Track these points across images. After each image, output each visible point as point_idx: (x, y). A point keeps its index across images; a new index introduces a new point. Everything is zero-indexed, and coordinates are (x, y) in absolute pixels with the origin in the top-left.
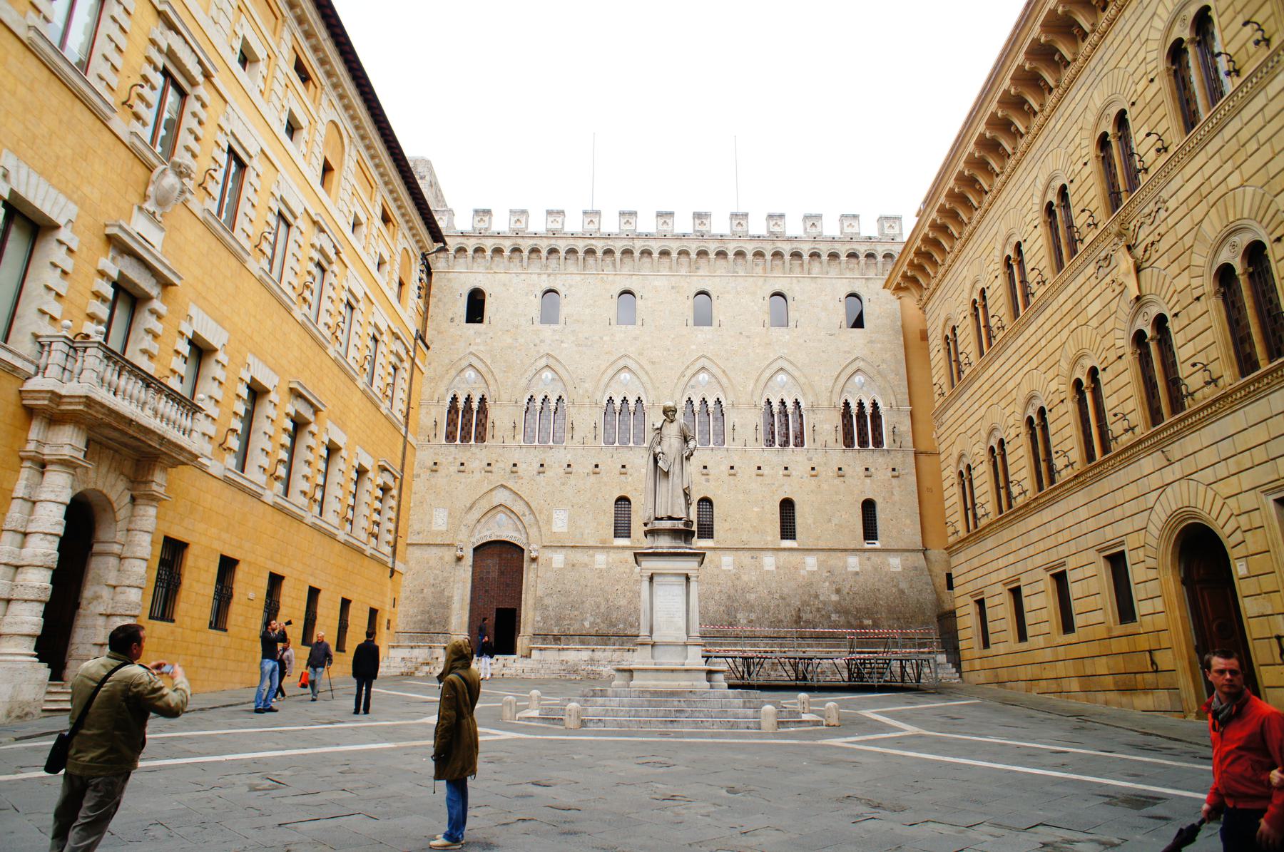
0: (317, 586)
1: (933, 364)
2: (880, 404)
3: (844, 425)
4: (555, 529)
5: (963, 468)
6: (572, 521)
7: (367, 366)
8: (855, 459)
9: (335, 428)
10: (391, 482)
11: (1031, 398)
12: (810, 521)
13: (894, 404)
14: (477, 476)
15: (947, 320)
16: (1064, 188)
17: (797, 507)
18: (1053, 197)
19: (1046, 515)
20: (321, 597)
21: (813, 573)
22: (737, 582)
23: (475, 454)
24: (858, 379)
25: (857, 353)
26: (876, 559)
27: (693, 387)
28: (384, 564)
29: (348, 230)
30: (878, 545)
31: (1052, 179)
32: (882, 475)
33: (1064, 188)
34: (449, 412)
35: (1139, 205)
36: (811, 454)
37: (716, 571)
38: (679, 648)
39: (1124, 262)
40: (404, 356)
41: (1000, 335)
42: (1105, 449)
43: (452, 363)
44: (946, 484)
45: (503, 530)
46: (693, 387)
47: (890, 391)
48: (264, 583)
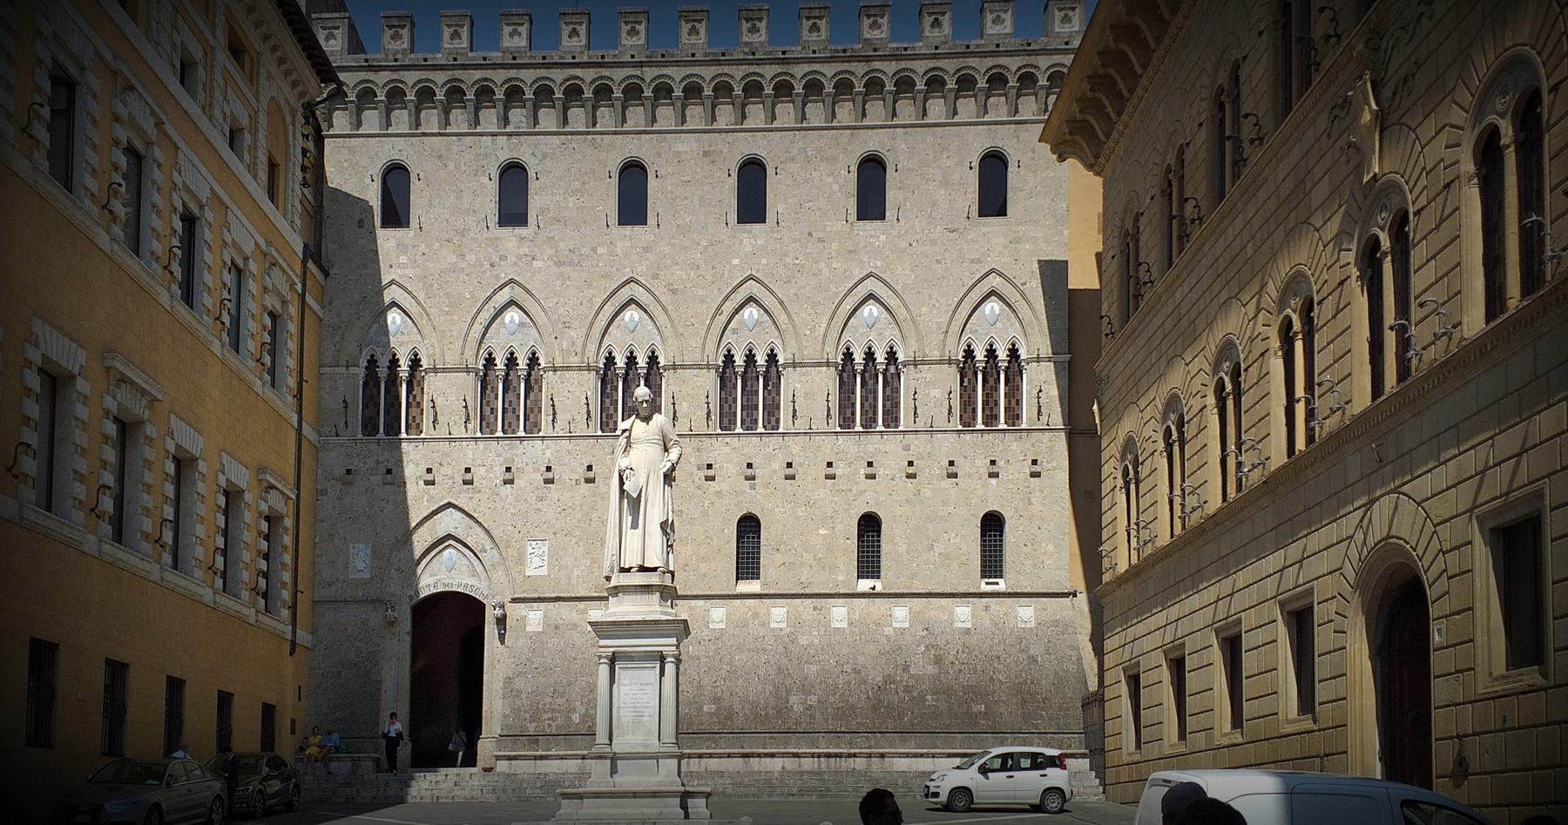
6: (554, 558)
12: (902, 549)
17: (885, 528)
27: (735, 331)
34: (365, 384)
46: (735, 331)
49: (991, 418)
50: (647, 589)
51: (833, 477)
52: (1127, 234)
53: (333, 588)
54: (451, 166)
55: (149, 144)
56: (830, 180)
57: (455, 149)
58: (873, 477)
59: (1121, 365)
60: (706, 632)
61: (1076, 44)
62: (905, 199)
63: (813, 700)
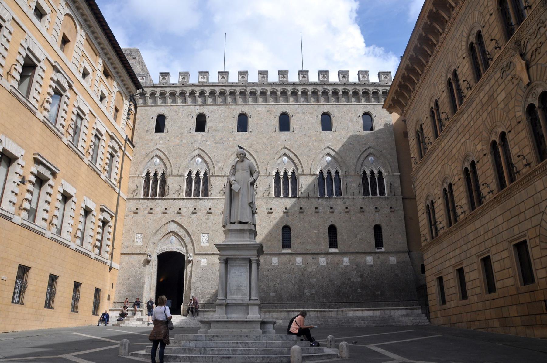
0: (55, 273)
1: (411, 147)
2: (383, 172)
3: (363, 184)
4: (202, 244)
5: (429, 203)
7: (91, 151)
8: (369, 204)
9: (68, 184)
10: (108, 218)
11: (465, 158)
12: (345, 237)
13: (390, 171)
14: (160, 215)
15: (417, 121)
16: (479, 33)
17: (338, 230)
18: (473, 39)
19: (478, 224)
20: (59, 281)
21: (347, 266)
22: (305, 272)
23: (159, 205)
24: (370, 158)
25: (370, 144)
26: (382, 257)
28: (106, 263)
29: (79, 76)
30: (383, 250)
31: (472, 29)
32: (385, 211)
33: (479, 33)
35: (526, 32)
36: (346, 200)
37: (293, 267)
38: (244, 307)
39: (519, 64)
40: (117, 147)
41: (447, 123)
42: (512, 180)
43: (147, 154)
44: (420, 214)
45: (175, 246)
47: (388, 164)
48: (15, 271)
49: (374, 193)
50: (242, 231)
51: (318, 212)
52: (418, 131)
53: (128, 249)
54: (180, 114)
55: (65, 91)
56: (312, 119)
57: (181, 109)
58: (333, 212)
59: (421, 172)
60: (271, 267)
61: (390, 84)
62: (338, 125)
63: (313, 291)
